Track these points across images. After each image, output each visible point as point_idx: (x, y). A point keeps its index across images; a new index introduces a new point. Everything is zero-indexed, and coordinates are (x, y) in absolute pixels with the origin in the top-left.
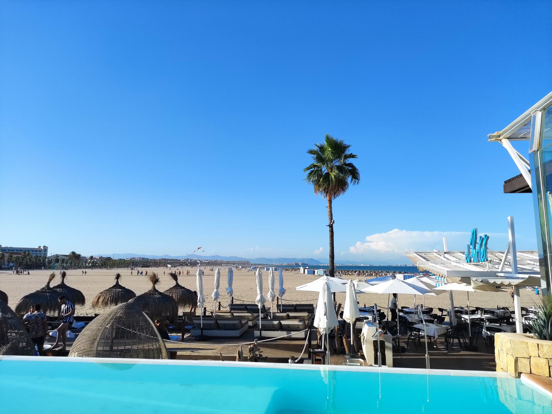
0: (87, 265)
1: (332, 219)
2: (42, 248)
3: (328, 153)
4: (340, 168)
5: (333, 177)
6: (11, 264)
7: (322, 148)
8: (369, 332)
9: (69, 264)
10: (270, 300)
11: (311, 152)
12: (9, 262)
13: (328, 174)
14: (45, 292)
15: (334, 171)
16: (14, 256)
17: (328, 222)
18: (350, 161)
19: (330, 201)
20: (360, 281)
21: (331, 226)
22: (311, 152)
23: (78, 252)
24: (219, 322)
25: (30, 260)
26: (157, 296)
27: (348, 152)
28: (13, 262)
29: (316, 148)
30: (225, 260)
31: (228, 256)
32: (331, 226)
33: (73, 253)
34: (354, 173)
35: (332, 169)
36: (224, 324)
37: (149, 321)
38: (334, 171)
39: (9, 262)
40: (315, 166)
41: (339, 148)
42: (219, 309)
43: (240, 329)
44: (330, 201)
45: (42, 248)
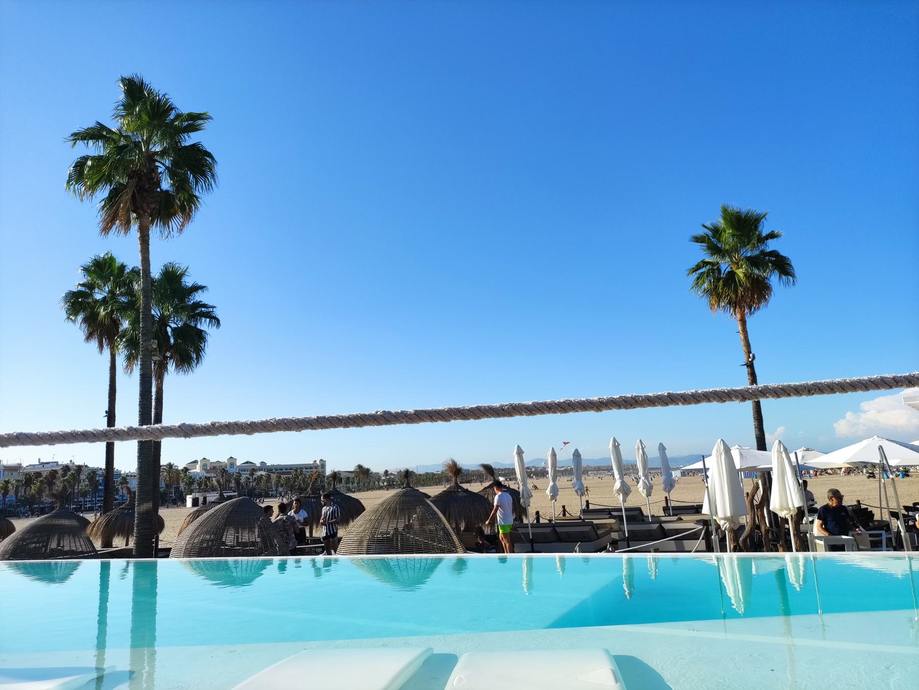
0: (381, 484)
1: (749, 352)
2: (318, 462)
3: (728, 235)
4: (754, 262)
5: (741, 275)
6: (281, 489)
7: (716, 231)
8: (817, 529)
9: (355, 485)
10: (644, 495)
11: (697, 239)
12: (277, 487)
13: (732, 274)
14: (309, 497)
15: (743, 267)
16: (283, 476)
17: (744, 359)
18: (771, 245)
19: (743, 322)
20: (808, 450)
21: (750, 366)
22: (697, 239)
23: (366, 466)
24: (559, 530)
25: (304, 481)
26: (460, 494)
27: (765, 231)
28: (282, 486)
29: (701, 232)
30: (593, 465)
31: (597, 457)
32: (750, 366)
33: (360, 467)
34: (783, 266)
35: (737, 264)
36: (567, 532)
37: (436, 513)
38: (743, 267)
39: (277, 487)
40: (705, 263)
41: (745, 226)
42: (564, 515)
43: (591, 541)
44: (743, 322)
45: (318, 462)
